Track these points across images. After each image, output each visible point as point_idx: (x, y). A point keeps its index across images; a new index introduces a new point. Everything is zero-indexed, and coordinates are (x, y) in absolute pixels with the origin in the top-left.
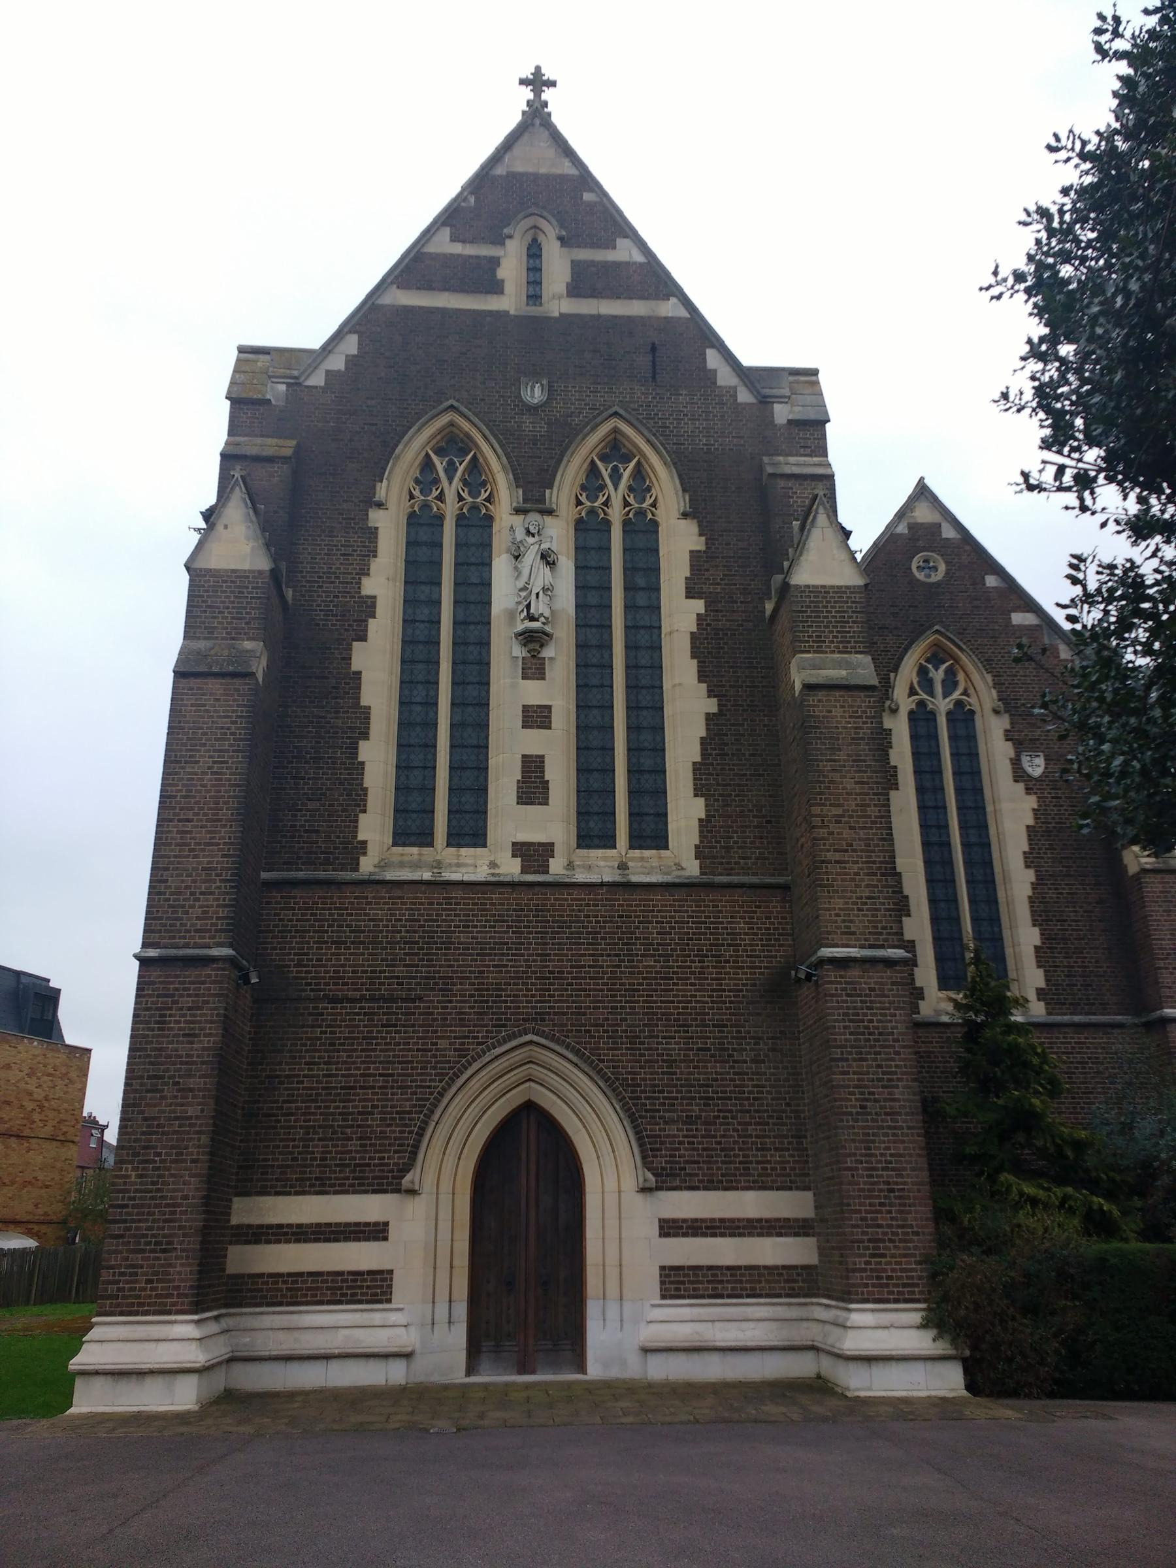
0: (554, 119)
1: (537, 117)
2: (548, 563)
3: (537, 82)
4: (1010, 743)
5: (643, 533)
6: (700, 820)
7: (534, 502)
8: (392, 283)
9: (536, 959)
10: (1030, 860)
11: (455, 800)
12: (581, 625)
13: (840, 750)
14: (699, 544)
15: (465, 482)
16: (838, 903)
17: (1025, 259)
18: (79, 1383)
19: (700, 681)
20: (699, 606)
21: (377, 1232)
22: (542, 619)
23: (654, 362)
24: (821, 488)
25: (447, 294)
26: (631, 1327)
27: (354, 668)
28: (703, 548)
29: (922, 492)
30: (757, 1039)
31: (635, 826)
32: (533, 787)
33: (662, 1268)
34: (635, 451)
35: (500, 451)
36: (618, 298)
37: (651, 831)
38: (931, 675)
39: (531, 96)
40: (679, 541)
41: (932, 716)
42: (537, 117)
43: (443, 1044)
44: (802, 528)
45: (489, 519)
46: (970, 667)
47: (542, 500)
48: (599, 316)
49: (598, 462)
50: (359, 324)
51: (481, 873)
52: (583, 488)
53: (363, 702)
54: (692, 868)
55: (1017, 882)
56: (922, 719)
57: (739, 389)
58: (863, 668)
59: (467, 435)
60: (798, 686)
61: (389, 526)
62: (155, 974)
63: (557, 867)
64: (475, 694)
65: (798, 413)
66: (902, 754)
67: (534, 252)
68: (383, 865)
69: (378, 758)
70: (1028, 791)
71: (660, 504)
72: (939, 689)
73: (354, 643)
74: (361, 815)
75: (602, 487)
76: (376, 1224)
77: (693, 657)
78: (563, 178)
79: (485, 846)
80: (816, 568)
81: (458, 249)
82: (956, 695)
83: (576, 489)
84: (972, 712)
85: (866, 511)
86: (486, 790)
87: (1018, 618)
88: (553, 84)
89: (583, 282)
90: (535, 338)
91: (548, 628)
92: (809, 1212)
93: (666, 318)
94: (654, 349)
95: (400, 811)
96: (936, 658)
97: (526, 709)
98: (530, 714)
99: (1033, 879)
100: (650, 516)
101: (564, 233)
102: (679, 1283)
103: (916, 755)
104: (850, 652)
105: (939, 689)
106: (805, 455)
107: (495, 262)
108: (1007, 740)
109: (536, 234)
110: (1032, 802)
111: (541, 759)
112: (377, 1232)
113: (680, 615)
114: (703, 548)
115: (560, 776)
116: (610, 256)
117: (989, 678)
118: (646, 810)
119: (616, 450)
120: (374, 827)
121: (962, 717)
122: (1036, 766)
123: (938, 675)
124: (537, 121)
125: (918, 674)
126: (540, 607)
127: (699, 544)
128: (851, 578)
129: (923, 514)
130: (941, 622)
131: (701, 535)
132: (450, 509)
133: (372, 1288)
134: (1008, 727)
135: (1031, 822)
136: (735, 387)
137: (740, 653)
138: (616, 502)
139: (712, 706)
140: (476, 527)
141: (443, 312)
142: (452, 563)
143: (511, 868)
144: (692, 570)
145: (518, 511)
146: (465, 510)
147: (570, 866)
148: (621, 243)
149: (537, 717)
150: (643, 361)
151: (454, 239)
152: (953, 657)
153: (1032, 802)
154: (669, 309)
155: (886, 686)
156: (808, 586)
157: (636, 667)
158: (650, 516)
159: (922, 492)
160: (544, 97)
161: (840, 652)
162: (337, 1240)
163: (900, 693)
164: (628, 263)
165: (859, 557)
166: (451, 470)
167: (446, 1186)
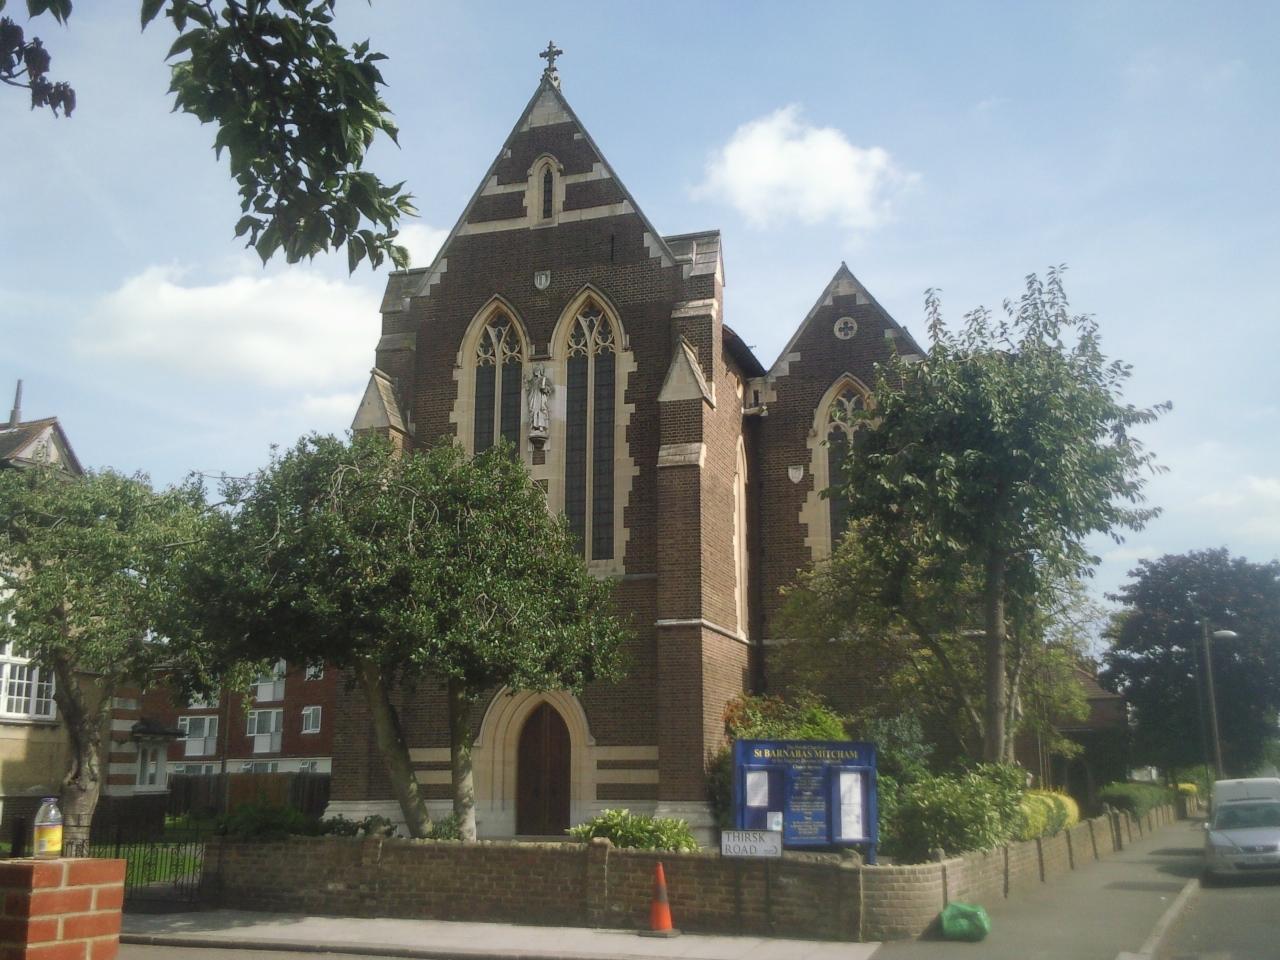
1: (548, 87)
5: (606, 361)
7: (542, 355)
17: (351, 46)
25: (495, 222)
26: (588, 813)
29: (844, 273)
35: (617, 313)
42: (548, 87)
61: (465, 377)
67: (548, 180)
89: (578, 197)
90: (548, 246)
107: (522, 194)
114: (635, 370)
116: (590, 177)
123: (849, 406)
124: (547, 86)
129: (844, 290)
140: (513, 369)
142: (501, 397)
148: (597, 167)
151: (500, 183)
152: (860, 393)
154: (623, 209)
159: (844, 273)
166: (591, 327)
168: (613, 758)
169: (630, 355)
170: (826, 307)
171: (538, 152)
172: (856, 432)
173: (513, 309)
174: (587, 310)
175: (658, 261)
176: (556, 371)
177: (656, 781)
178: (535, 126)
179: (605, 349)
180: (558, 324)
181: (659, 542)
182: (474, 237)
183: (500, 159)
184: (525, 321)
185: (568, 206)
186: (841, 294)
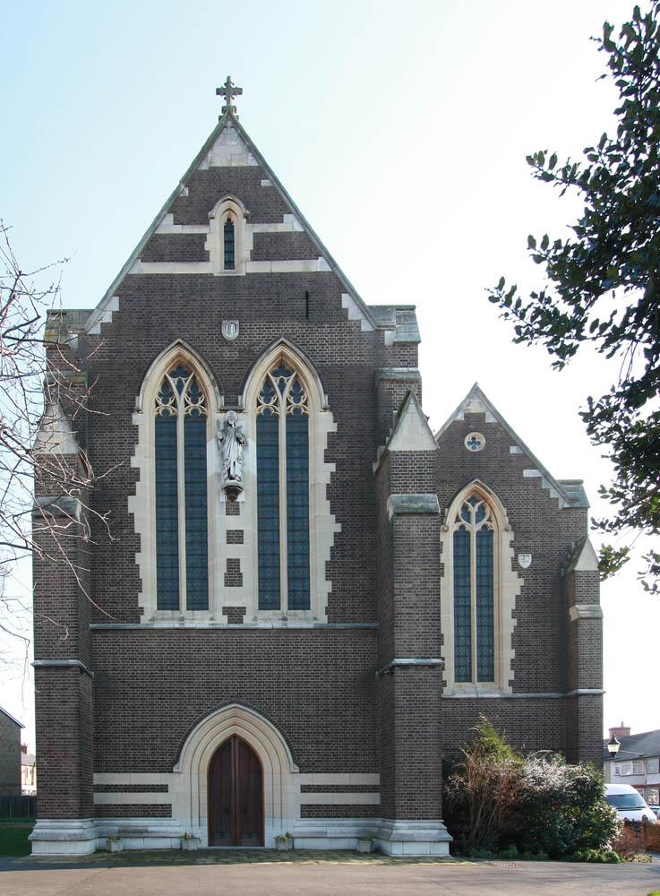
0: (241, 122)
1: (229, 119)
2: (240, 443)
3: (228, 91)
4: (512, 549)
5: (299, 423)
6: (329, 594)
7: (232, 400)
8: (138, 258)
9: (233, 666)
10: (514, 614)
11: (190, 585)
12: (260, 481)
13: (413, 551)
14: (333, 428)
15: (189, 394)
16: (406, 635)
18: (33, 843)
19: (331, 513)
20: (332, 467)
21: (163, 789)
22: (237, 478)
23: (307, 305)
24: (412, 391)
27: (130, 511)
28: (336, 430)
29: (476, 391)
30: (355, 705)
31: (292, 597)
32: (234, 576)
33: (302, 805)
34: (294, 368)
36: (285, 260)
37: (300, 601)
38: (470, 509)
39: (224, 103)
40: (322, 425)
41: (468, 534)
42: (229, 119)
43: (189, 708)
44: (399, 415)
45: (204, 417)
46: (494, 504)
47: (236, 403)
48: (272, 273)
49: (271, 377)
50: (118, 289)
51: (206, 624)
52: (262, 394)
53: (136, 531)
54: (323, 619)
55: (506, 624)
56: (461, 537)
57: (363, 321)
58: (432, 501)
59: (189, 362)
60: (391, 514)
61: (145, 421)
62: (42, 673)
63: (248, 620)
64: (199, 524)
65: (403, 337)
66: (447, 557)
67: (229, 229)
68: (153, 619)
69: (147, 562)
70: (520, 576)
71: (310, 403)
72: (473, 518)
73: (129, 497)
74: (139, 594)
75: (274, 393)
76: (162, 785)
77: (327, 499)
78: (250, 169)
79: (207, 609)
80: (407, 439)
81: (178, 229)
82: (484, 521)
83: (258, 395)
84: (492, 531)
85: (439, 405)
86: (207, 579)
87: (527, 473)
88: (239, 91)
89: (266, 248)
90: (233, 294)
91: (241, 484)
92: (378, 783)
93: (315, 272)
94: (307, 295)
95: (160, 592)
96: (473, 500)
97: (229, 532)
98: (233, 532)
99: (516, 624)
100: (303, 411)
101: (248, 212)
102: (308, 811)
103: (456, 557)
104: (424, 493)
105: (473, 518)
106: (404, 367)
107: (203, 237)
108: (511, 547)
109: (229, 214)
110: (521, 582)
111: (238, 561)
112: (163, 789)
113: (321, 473)
115: (250, 571)
116: (280, 228)
117: (505, 510)
118: (298, 589)
119: (282, 368)
120: (148, 599)
121: (486, 536)
122: (526, 561)
123: (473, 510)
124: (229, 123)
125: (462, 509)
126: (236, 471)
127: (333, 428)
128: (427, 445)
129: (475, 408)
130: (479, 477)
131: (335, 422)
132: (181, 412)
133: (164, 811)
134: (513, 539)
135: (519, 593)
136: (360, 321)
137: (360, 492)
138: (283, 403)
139: (338, 528)
140: (197, 423)
141: (171, 276)
142: (184, 446)
143: (222, 621)
144: (328, 444)
145: (222, 411)
146: (189, 412)
147: (255, 619)
148: (288, 218)
149: (235, 537)
150: (301, 305)
151: (176, 222)
153: (521, 582)
154: (319, 265)
155: (443, 516)
156: (401, 452)
157: (293, 506)
158: (303, 411)
159: (476, 391)
160: (233, 103)
161: (418, 493)
162: (143, 792)
163: (450, 519)
164: (291, 233)
165: (434, 434)
166: (180, 387)
167: (195, 770)
168: (347, 783)
169: (328, 416)
170: (459, 422)
171: (221, 193)
172: (478, 532)
173: (199, 357)
174: (277, 368)
175: (358, 324)
176: (247, 423)
177: (378, 802)
178: (213, 165)
179: (297, 410)
180: (250, 377)
181: (397, 586)
182: (150, 277)
183: (176, 197)
184: (212, 369)
185: (257, 255)
186: (472, 412)
